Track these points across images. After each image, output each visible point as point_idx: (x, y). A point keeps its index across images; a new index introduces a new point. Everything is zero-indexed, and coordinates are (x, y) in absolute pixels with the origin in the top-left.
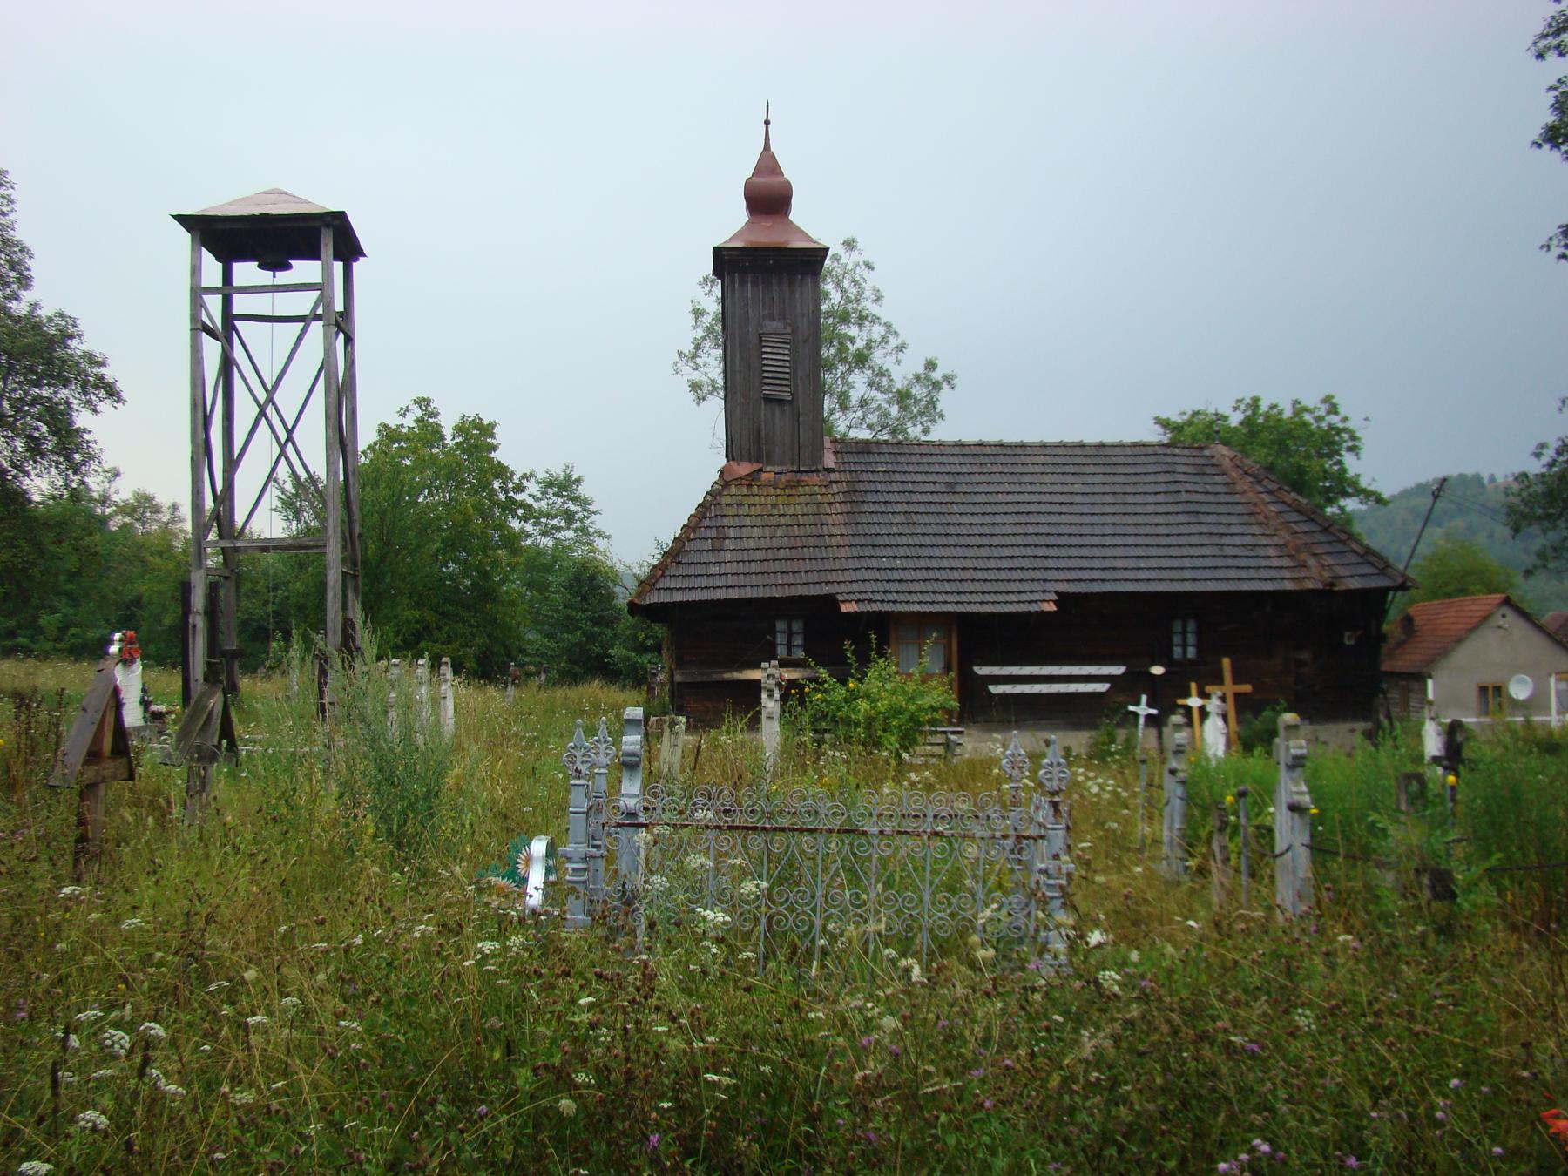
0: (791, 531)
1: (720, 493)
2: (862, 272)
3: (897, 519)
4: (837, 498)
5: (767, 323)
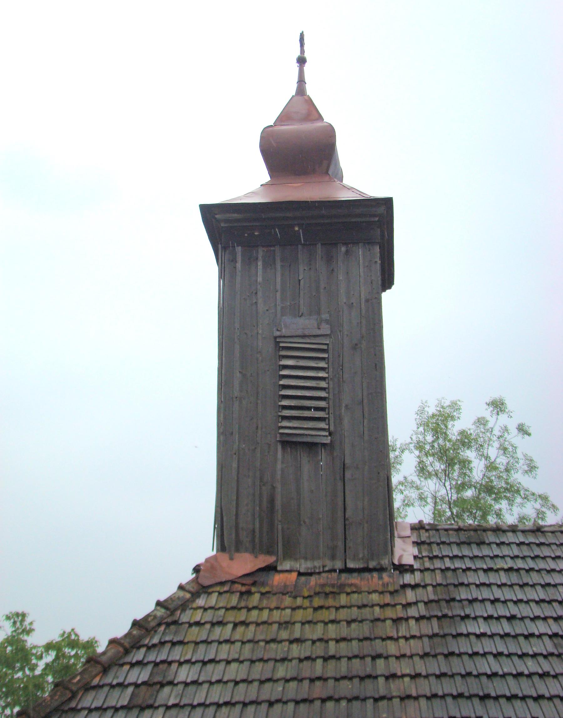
0: (307, 670)
1: (184, 606)
2: (514, 437)
3: (537, 647)
4: (413, 612)
5: (288, 319)
